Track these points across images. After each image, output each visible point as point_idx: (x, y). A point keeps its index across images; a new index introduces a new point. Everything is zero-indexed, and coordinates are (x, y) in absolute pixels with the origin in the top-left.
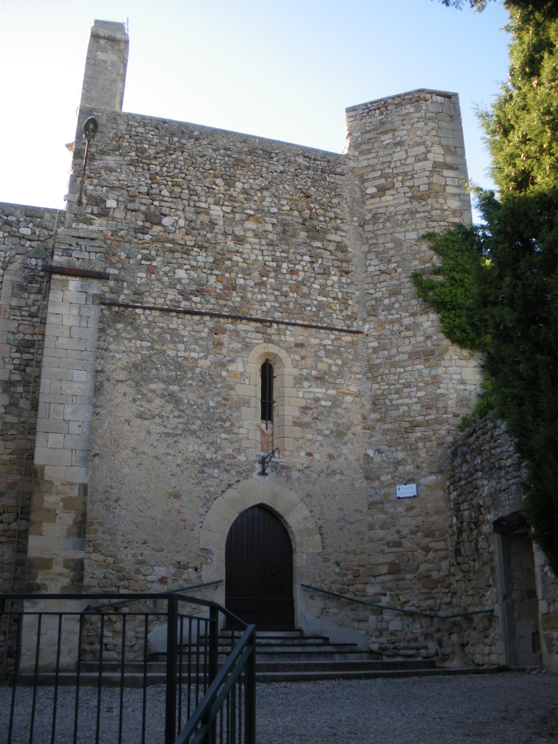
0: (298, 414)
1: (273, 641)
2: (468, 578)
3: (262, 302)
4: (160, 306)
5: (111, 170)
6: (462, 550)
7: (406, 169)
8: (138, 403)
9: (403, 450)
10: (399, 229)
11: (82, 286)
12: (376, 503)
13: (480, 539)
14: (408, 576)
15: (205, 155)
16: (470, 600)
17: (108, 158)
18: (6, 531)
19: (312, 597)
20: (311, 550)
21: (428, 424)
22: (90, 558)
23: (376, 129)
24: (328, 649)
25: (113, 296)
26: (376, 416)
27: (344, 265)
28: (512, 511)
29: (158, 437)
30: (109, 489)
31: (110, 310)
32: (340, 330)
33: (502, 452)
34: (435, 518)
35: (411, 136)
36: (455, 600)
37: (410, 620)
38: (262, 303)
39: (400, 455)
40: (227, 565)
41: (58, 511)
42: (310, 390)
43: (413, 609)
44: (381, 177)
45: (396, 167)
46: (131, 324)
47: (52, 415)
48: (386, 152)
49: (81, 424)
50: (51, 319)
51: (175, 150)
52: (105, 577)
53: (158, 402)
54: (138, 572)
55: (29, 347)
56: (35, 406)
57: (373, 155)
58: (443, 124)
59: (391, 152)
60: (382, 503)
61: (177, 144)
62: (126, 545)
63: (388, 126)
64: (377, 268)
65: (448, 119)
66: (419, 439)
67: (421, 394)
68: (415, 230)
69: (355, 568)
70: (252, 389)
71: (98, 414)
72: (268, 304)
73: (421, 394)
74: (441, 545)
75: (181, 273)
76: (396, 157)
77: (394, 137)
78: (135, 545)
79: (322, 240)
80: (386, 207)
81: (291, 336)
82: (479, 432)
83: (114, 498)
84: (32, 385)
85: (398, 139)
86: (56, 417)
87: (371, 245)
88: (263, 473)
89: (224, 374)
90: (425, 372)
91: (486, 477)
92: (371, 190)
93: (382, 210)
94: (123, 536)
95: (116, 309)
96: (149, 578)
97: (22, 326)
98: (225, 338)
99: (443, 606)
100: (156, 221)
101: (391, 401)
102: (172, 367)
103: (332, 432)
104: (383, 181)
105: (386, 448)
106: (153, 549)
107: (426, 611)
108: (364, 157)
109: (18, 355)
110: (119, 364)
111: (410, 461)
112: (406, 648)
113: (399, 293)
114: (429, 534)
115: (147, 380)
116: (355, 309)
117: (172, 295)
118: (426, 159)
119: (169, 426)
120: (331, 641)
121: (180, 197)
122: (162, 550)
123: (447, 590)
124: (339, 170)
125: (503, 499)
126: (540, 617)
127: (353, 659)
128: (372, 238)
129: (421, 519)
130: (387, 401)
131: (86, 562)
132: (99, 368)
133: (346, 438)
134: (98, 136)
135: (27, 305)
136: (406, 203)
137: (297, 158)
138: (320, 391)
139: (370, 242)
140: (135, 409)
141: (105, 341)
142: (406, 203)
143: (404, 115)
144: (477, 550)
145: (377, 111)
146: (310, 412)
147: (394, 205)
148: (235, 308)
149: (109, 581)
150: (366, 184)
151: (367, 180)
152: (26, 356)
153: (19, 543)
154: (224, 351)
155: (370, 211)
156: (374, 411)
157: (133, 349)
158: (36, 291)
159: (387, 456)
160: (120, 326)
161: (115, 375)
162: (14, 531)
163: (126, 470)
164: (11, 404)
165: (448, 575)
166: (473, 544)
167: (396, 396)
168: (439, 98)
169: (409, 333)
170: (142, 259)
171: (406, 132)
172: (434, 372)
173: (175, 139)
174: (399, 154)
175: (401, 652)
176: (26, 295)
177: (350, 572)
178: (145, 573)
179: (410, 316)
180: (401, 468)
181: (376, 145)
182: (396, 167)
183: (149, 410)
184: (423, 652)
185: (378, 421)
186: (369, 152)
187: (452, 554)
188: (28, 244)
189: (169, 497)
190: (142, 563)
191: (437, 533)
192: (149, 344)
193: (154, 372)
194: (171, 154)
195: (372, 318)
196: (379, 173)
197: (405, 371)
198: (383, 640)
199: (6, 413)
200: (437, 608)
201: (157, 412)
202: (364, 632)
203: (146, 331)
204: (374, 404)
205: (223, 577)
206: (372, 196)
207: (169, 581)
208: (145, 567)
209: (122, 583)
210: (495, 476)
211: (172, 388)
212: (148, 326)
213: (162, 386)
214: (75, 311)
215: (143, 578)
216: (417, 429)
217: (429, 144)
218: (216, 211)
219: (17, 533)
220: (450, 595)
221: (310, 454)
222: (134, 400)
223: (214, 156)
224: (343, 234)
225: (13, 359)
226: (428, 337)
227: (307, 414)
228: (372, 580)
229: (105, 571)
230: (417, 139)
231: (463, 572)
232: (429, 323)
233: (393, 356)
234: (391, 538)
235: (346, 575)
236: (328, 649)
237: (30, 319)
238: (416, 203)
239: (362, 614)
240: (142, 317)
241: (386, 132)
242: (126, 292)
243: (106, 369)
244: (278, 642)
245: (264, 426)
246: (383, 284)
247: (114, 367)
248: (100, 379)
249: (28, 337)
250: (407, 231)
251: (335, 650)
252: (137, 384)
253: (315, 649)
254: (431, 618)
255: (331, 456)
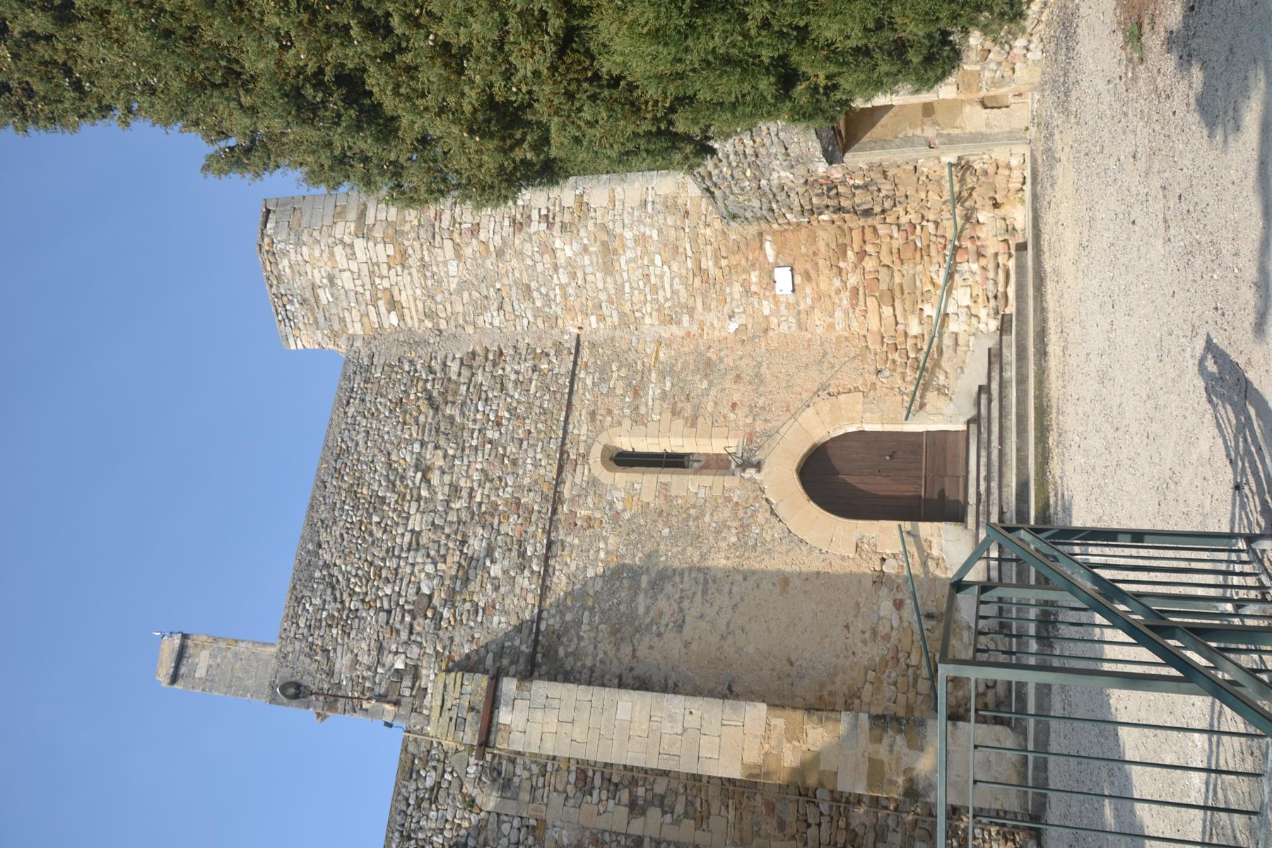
0: (681, 422)
1: (983, 460)
2: (903, 199)
3: (536, 465)
4: (538, 598)
5: (356, 662)
6: (866, 207)
7: (365, 272)
8: (662, 630)
9: (730, 285)
10: (445, 284)
11: (506, 705)
12: (799, 321)
13: (851, 182)
14: (897, 279)
15: (342, 535)
16: (933, 196)
17: (338, 666)
18: (832, 818)
19: (922, 406)
20: (859, 407)
21: (697, 254)
22: (869, 704)
23: (312, 311)
24: (995, 387)
25: (522, 660)
26: (686, 318)
27: (491, 357)
28: (814, 136)
29: (708, 605)
30: (775, 674)
31: (540, 665)
32: (575, 363)
33: (736, 153)
34: (822, 246)
35: (322, 264)
36: (931, 216)
37: (957, 276)
38: (536, 466)
39: (737, 289)
40: (878, 519)
41: (804, 748)
42: (650, 403)
43: (942, 273)
44: (376, 306)
45: (363, 286)
46: (559, 637)
47: (674, 751)
48: (343, 297)
49: (687, 712)
50: (549, 749)
51: (331, 576)
52: (895, 684)
53: (662, 603)
54: (887, 638)
55: (586, 776)
56: (665, 773)
57: (347, 314)
58: (304, 223)
59: (342, 291)
60: (799, 313)
61: (325, 572)
62: (850, 653)
63: (308, 294)
64: (495, 314)
65: (298, 213)
66: (716, 263)
67: (658, 261)
68: (445, 263)
69: (885, 349)
70: (647, 482)
71: (676, 685)
72: (539, 456)
73: (658, 261)
74: (856, 235)
75: (495, 570)
76: (349, 285)
77: (324, 287)
78: (850, 641)
79: (457, 383)
80: (415, 300)
81: (581, 429)
82: (709, 183)
83: (788, 666)
84: (635, 774)
85: (325, 281)
86: (678, 745)
87: (466, 321)
88: (758, 466)
89: (627, 515)
90: (629, 254)
91: (767, 174)
92: (394, 318)
93: (420, 306)
94: (838, 657)
95: (539, 656)
96: (895, 624)
97: (558, 786)
98: (582, 512)
99: (940, 232)
100: (425, 600)
101: (666, 300)
102: (617, 583)
103: (706, 376)
104: (382, 305)
105: (727, 306)
106: (856, 616)
107: (945, 255)
108: (349, 326)
109: (595, 793)
110: (611, 654)
111: (744, 277)
112: (996, 283)
113: (528, 287)
114: (842, 250)
115: (633, 615)
116: (549, 344)
117: (523, 581)
118: (352, 246)
119: (693, 589)
120: (984, 382)
121: (396, 570)
122: (858, 604)
123: (918, 227)
124: (366, 361)
125: (797, 151)
126: (962, 97)
127: (1010, 355)
128: (456, 320)
129: (821, 262)
130: (667, 305)
131: (874, 711)
132: (616, 681)
133: (714, 357)
134: (307, 681)
135: (530, 779)
136: (410, 274)
137: (350, 415)
138: (653, 391)
139: (461, 322)
140: (670, 635)
141: (580, 673)
142: (410, 274)
143: (293, 272)
144: (865, 187)
145: (288, 307)
146: (680, 405)
147: (414, 288)
148: (545, 498)
149: (900, 680)
150: (386, 325)
151: (381, 325)
152: (597, 782)
153: (848, 802)
154: (598, 515)
155: (420, 321)
156: (679, 323)
157: (592, 635)
158: (511, 766)
159: (738, 307)
160: (561, 652)
161: (626, 660)
162: (831, 807)
163: (751, 649)
164: (662, 806)
165: (899, 226)
166: (857, 192)
167: (661, 293)
168: (269, 226)
169: (580, 275)
170: (475, 621)
171: (316, 271)
172: (630, 244)
173: (317, 574)
174: (345, 281)
175: (1001, 289)
176: (516, 780)
177: (890, 357)
178: (888, 629)
179: (1262, 802)
180: (754, 288)
181: (334, 311)
182: (363, 286)
183: (672, 615)
184: (1001, 260)
185: (691, 317)
186: (342, 320)
187: (870, 221)
188: (448, 776)
189: (787, 593)
190: (874, 633)
191: (840, 241)
192: (587, 613)
193: (622, 607)
194: (338, 581)
195: (560, 322)
196: (371, 308)
197: (629, 281)
198: (983, 313)
199: (672, 813)
200: (942, 241)
201: (675, 606)
202: (972, 338)
203: (569, 617)
204: (670, 322)
205: (895, 523)
206: (402, 317)
207: (900, 596)
208: (881, 628)
209: (902, 660)
210: (766, 161)
211: (644, 585)
212: (562, 614)
213: (641, 598)
214: (538, 715)
215: (894, 633)
216: (703, 267)
217: (331, 240)
218: (416, 523)
219: (835, 804)
220: (924, 223)
221: (734, 406)
222: (659, 635)
223: (341, 524)
224: (450, 357)
225: (601, 800)
226: (585, 249)
227: (682, 409)
228: (900, 327)
229: (885, 684)
230: (325, 255)
231: (895, 205)
232: (567, 248)
233: (609, 295)
234: (845, 302)
235: (894, 362)
236: (995, 387)
237: (548, 775)
238: (410, 261)
239: (947, 341)
240: (551, 622)
241: (316, 297)
242: (517, 643)
243: (617, 672)
244: (983, 453)
245: (696, 465)
246: (516, 307)
247: (615, 661)
248: (630, 681)
249: (572, 778)
250: (447, 273)
251: (997, 377)
252: (637, 630)
253: (995, 405)
254: (956, 249)
255: (738, 378)
